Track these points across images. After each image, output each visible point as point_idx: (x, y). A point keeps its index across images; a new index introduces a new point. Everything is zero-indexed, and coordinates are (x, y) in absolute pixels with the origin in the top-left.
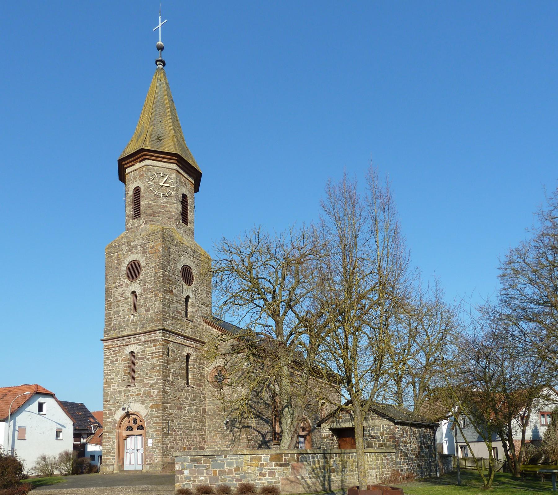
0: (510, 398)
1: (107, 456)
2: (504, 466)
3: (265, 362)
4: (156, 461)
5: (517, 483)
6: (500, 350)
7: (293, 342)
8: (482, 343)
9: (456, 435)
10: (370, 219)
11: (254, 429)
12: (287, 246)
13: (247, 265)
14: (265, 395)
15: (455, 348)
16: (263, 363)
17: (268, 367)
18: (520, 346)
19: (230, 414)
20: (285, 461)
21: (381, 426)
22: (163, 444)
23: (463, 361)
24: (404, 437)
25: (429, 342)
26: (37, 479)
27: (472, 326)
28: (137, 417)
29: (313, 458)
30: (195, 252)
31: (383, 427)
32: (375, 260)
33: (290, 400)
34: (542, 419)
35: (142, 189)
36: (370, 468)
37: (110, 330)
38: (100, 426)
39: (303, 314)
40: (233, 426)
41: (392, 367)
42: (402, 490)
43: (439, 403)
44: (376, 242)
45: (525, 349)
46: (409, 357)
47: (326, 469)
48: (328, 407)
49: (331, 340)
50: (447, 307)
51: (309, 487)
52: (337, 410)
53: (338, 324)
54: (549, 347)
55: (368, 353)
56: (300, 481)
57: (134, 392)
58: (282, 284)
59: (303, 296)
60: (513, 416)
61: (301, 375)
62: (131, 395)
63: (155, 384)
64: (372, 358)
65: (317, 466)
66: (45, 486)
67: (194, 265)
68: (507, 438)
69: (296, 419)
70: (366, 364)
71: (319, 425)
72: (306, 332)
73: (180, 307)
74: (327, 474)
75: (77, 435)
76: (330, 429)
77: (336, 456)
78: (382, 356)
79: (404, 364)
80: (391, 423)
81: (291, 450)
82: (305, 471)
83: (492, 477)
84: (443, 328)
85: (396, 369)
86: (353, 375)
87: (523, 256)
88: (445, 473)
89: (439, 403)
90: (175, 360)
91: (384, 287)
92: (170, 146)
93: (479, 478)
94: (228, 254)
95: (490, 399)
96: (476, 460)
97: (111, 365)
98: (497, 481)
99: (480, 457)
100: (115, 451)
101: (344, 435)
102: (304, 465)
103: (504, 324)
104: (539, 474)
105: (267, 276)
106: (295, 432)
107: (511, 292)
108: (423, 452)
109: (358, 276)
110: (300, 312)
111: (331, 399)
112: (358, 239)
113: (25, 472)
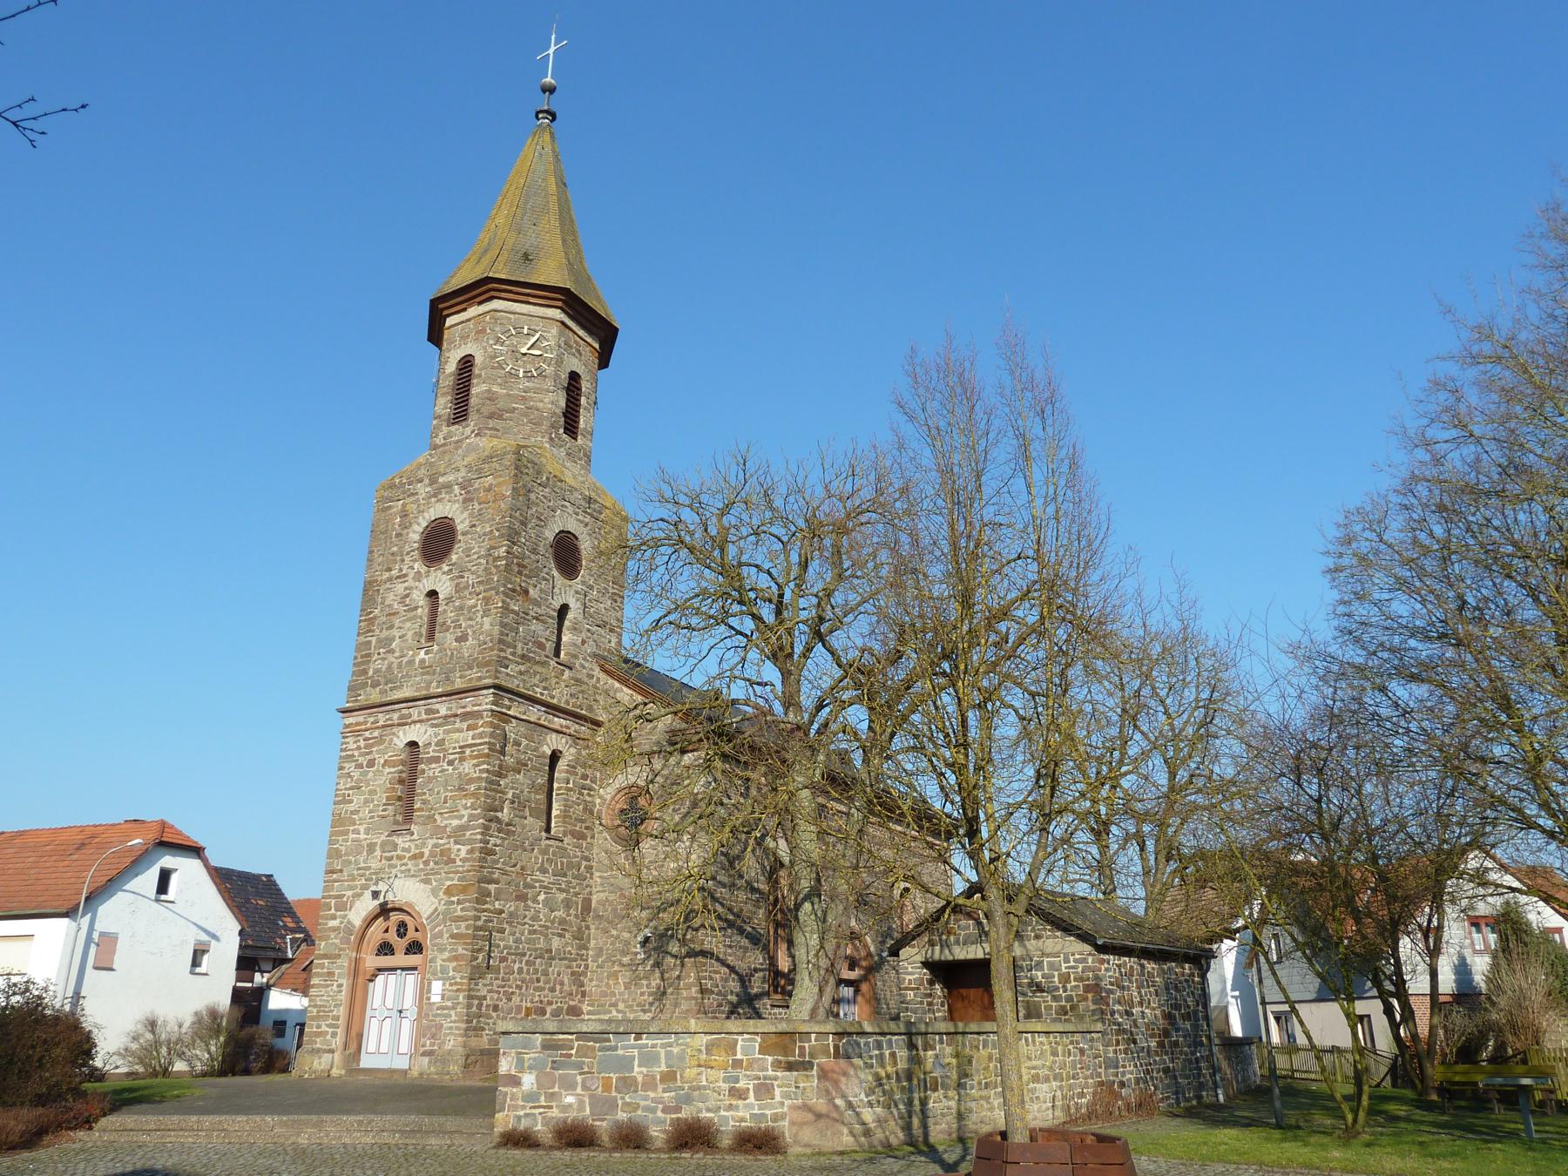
0: (1388, 879)
1: (319, 1027)
2: (1393, 1070)
3: (753, 776)
4: (449, 1046)
5: (1431, 1117)
6: (1351, 752)
7: (826, 725)
8: (1304, 734)
9: (1260, 981)
10: (1010, 434)
11: (718, 959)
12: (813, 492)
13: (714, 532)
14: (751, 866)
15: (1238, 748)
16: (748, 780)
17: (759, 789)
18: (1397, 742)
19: (655, 917)
20: (802, 1054)
21: (1061, 957)
22: (470, 997)
23: (1263, 782)
24: (1123, 988)
25: (1173, 730)
26: (127, 1083)
27: (1275, 690)
28: (407, 918)
29: (879, 1046)
30: (590, 500)
31: (1067, 960)
32: (1026, 527)
33: (818, 880)
34: (1476, 936)
35: (478, 360)
36: (1036, 1079)
37: (364, 685)
38: (309, 940)
39: (853, 654)
40: (661, 950)
41: (1083, 795)
42: (1126, 1143)
43: (1210, 894)
44: (1028, 486)
45: (1410, 751)
46: (1124, 769)
47: (914, 1081)
48: (918, 902)
49: (923, 723)
50: (1210, 644)
51: (867, 1133)
52: (943, 909)
53: (942, 680)
54: (1467, 745)
55: (1020, 758)
56: (841, 1114)
57: (408, 850)
58: (800, 581)
59: (852, 610)
60: (1402, 927)
61: (848, 814)
62: (400, 858)
63: (463, 828)
64: (1030, 771)
65: (889, 1069)
66: (144, 1106)
67: (585, 531)
68: (1392, 988)
69: (832, 934)
70: (1015, 785)
71: (895, 953)
72: (859, 700)
73: (544, 632)
74: (916, 1095)
75: (246, 963)
76: (926, 964)
77: (941, 1042)
78: (1056, 765)
79: (1114, 787)
80: (1088, 948)
81: (818, 1022)
82: (855, 1086)
83: (1365, 1101)
84: (1205, 695)
85: (1094, 802)
86: (982, 816)
87: (1377, 525)
88: (1240, 1092)
89: (1210, 894)
90: (520, 766)
91: (1052, 590)
92: (550, 272)
93: (1331, 1104)
94: (670, 506)
95: (1339, 883)
96: (1318, 1052)
97: (356, 774)
98: (1380, 1113)
99: (1328, 1043)
100: (342, 1011)
101: (963, 981)
102: (855, 1067)
103: (1353, 688)
104: (1486, 1092)
105: (763, 562)
106: (831, 970)
107: (1361, 610)
108: (1177, 1030)
109: (987, 565)
110: (846, 650)
111: (926, 879)
112: (983, 479)
113: (98, 1063)
